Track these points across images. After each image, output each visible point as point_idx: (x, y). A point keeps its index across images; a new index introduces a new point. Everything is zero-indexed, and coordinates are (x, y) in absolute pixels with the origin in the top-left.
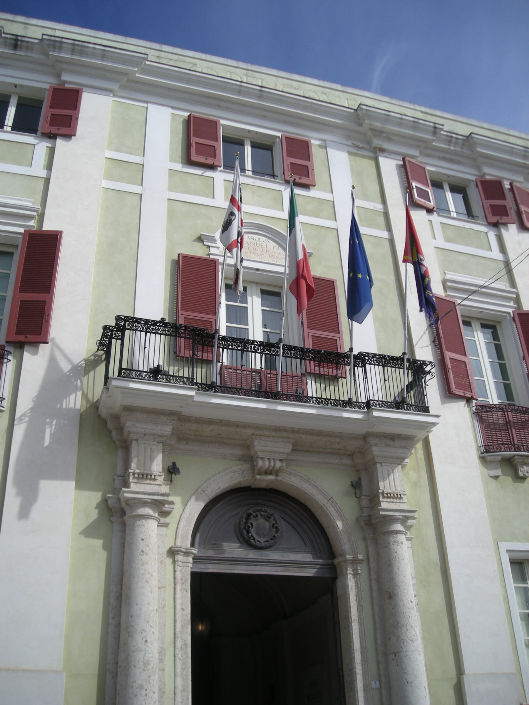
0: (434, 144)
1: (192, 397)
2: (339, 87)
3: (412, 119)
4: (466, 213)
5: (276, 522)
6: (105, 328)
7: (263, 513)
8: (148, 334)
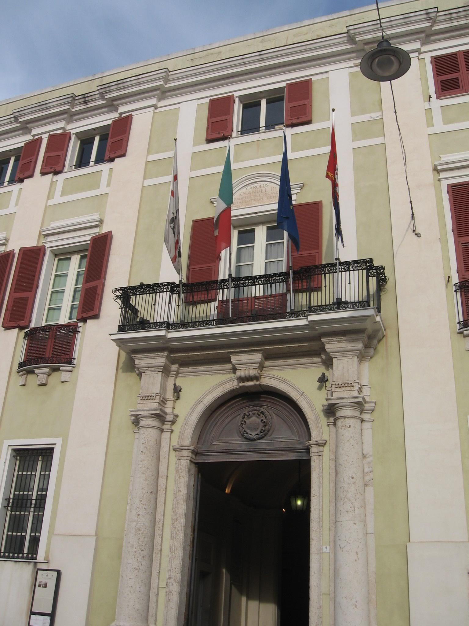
0: (433, 29)
2: (347, 13)
3: (402, 17)
4: (228, 140)
6: (371, 260)
7: (254, 412)
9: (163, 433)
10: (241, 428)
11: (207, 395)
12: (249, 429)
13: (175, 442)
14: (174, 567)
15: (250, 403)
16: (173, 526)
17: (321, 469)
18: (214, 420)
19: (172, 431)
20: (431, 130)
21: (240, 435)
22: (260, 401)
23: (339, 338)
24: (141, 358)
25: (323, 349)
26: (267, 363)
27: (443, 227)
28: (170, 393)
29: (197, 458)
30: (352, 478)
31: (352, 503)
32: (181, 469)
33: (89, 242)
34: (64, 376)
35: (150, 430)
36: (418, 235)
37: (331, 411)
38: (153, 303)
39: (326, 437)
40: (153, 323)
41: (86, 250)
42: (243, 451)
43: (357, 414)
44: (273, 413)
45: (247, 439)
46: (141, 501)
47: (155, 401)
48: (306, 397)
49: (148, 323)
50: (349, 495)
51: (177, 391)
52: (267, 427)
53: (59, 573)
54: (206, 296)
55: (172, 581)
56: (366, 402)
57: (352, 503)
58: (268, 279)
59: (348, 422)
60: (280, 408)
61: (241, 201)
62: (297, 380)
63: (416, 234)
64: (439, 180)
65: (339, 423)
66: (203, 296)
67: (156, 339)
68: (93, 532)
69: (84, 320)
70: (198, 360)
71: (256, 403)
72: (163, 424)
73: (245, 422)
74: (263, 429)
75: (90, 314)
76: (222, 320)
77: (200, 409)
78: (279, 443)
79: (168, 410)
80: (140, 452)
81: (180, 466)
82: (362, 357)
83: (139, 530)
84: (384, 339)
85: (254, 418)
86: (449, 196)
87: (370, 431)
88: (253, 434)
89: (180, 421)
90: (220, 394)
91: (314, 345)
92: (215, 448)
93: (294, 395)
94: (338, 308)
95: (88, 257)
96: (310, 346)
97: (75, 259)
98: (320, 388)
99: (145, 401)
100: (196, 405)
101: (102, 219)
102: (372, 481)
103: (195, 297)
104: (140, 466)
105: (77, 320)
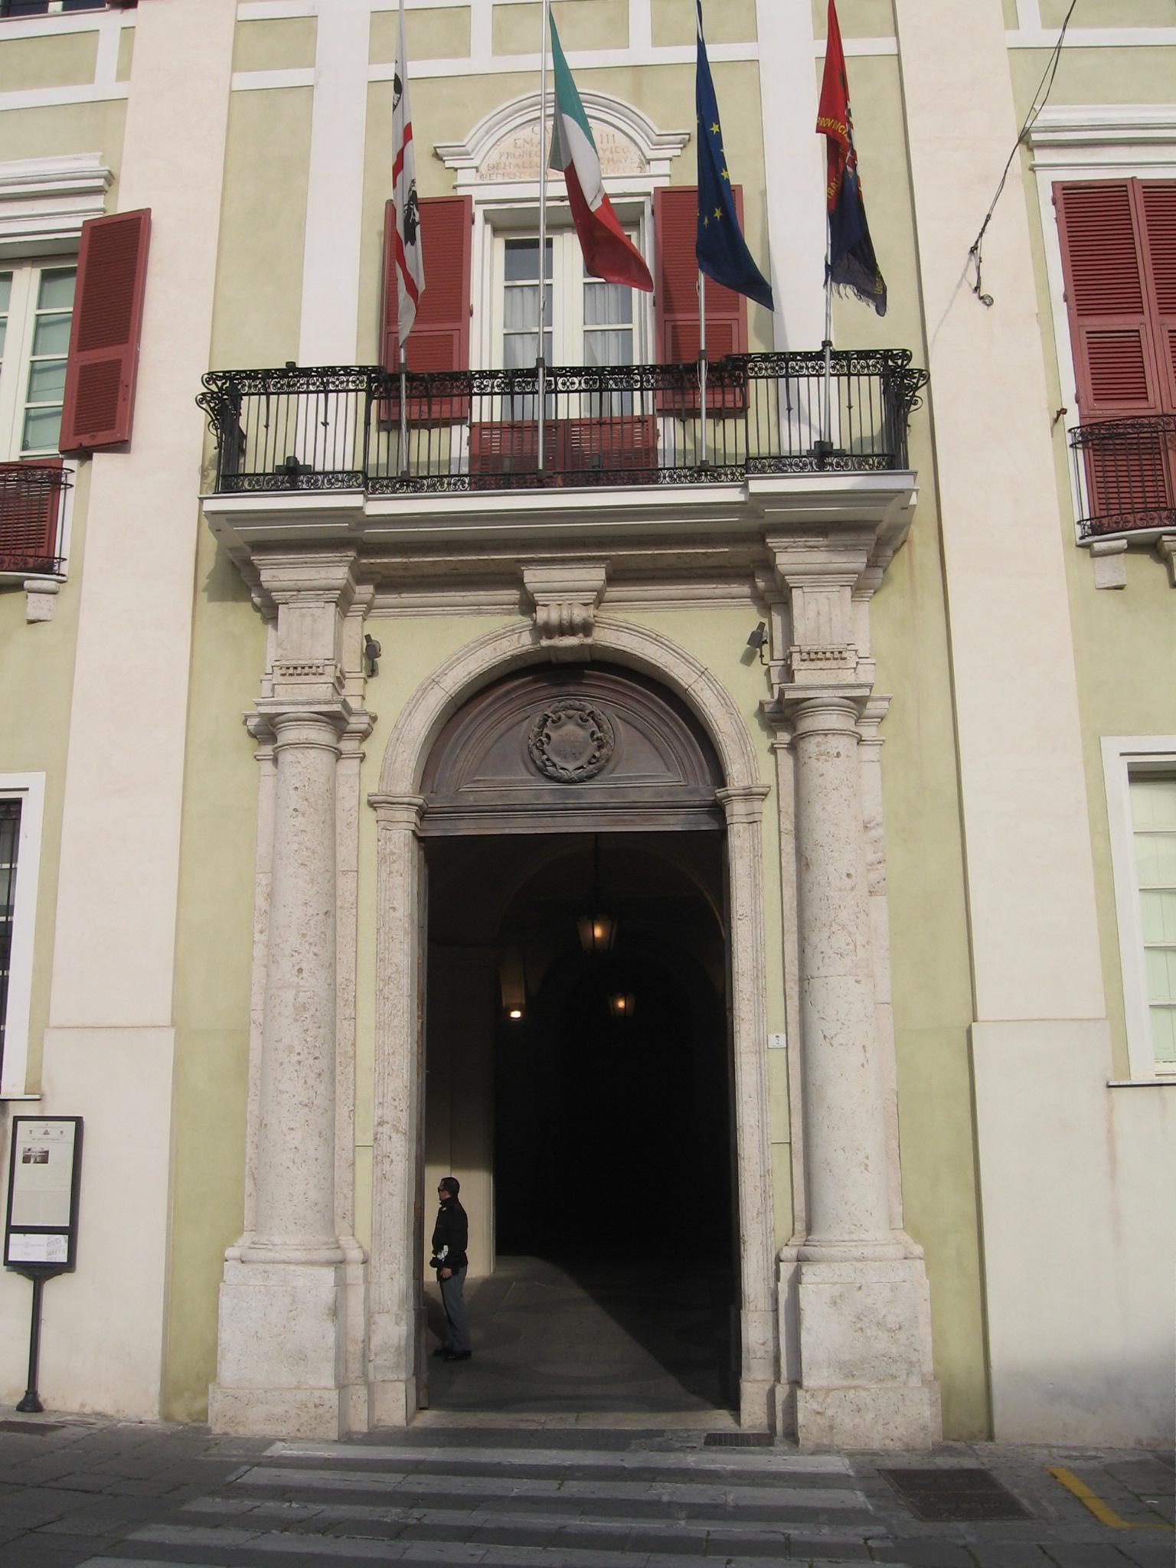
1: (360, 509)
5: (543, 725)
7: (571, 712)
8: (273, 398)
9: (342, 762)
10: (536, 752)
11: (450, 667)
12: (559, 753)
13: (372, 787)
14: (390, 1095)
15: (555, 691)
16: (381, 996)
17: (757, 855)
18: (466, 728)
19: (362, 759)
20: (1013, 38)
21: (533, 769)
22: (582, 684)
23: (813, 541)
24: (280, 565)
25: (768, 565)
26: (613, 592)
27: (1044, 286)
28: (353, 662)
29: (426, 825)
30: (849, 875)
31: (850, 933)
32: (392, 853)
33: (79, 234)
34: (36, 605)
35: (313, 753)
36: (987, 301)
37: (784, 716)
38: (321, 419)
39: (766, 778)
40: (325, 473)
41: (73, 255)
42: (550, 810)
43: (848, 724)
44: (617, 716)
45: (552, 778)
46: (304, 935)
47: (322, 679)
48: (712, 681)
49: (309, 471)
50: (844, 916)
51: (372, 651)
52: (604, 751)
53: (78, 1121)
54: (425, 408)
55: (386, 1129)
56: (350, 712)
57: (850, 933)
58: (596, 378)
59: (835, 743)
60: (634, 704)
61: (519, 161)
62: (697, 640)
63: (981, 298)
64: (1032, 169)
65: (811, 746)
66: (729, 397)
67: (298, 518)
68: (164, 1016)
69: (84, 454)
70: (428, 576)
71: (572, 689)
72: (339, 739)
73: (548, 736)
74: (597, 754)
75: (102, 437)
76: (489, 471)
77: (435, 702)
78: (637, 788)
79: (354, 704)
80: (291, 810)
81: (390, 847)
82: (861, 588)
83: (304, 1007)
84: (905, 547)
85: (570, 728)
86: (1057, 211)
87: (877, 767)
88: (570, 768)
89: (382, 732)
90: (486, 666)
91: (743, 553)
92: (470, 800)
93: (681, 674)
94: (821, 467)
95: (82, 273)
96: (739, 556)
97: (26, 281)
98: (748, 659)
99: (293, 680)
100: (424, 691)
101: (114, 171)
102: (883, 883)
103: (435, 408)
104: (295, 846)
105: (62, 452)
